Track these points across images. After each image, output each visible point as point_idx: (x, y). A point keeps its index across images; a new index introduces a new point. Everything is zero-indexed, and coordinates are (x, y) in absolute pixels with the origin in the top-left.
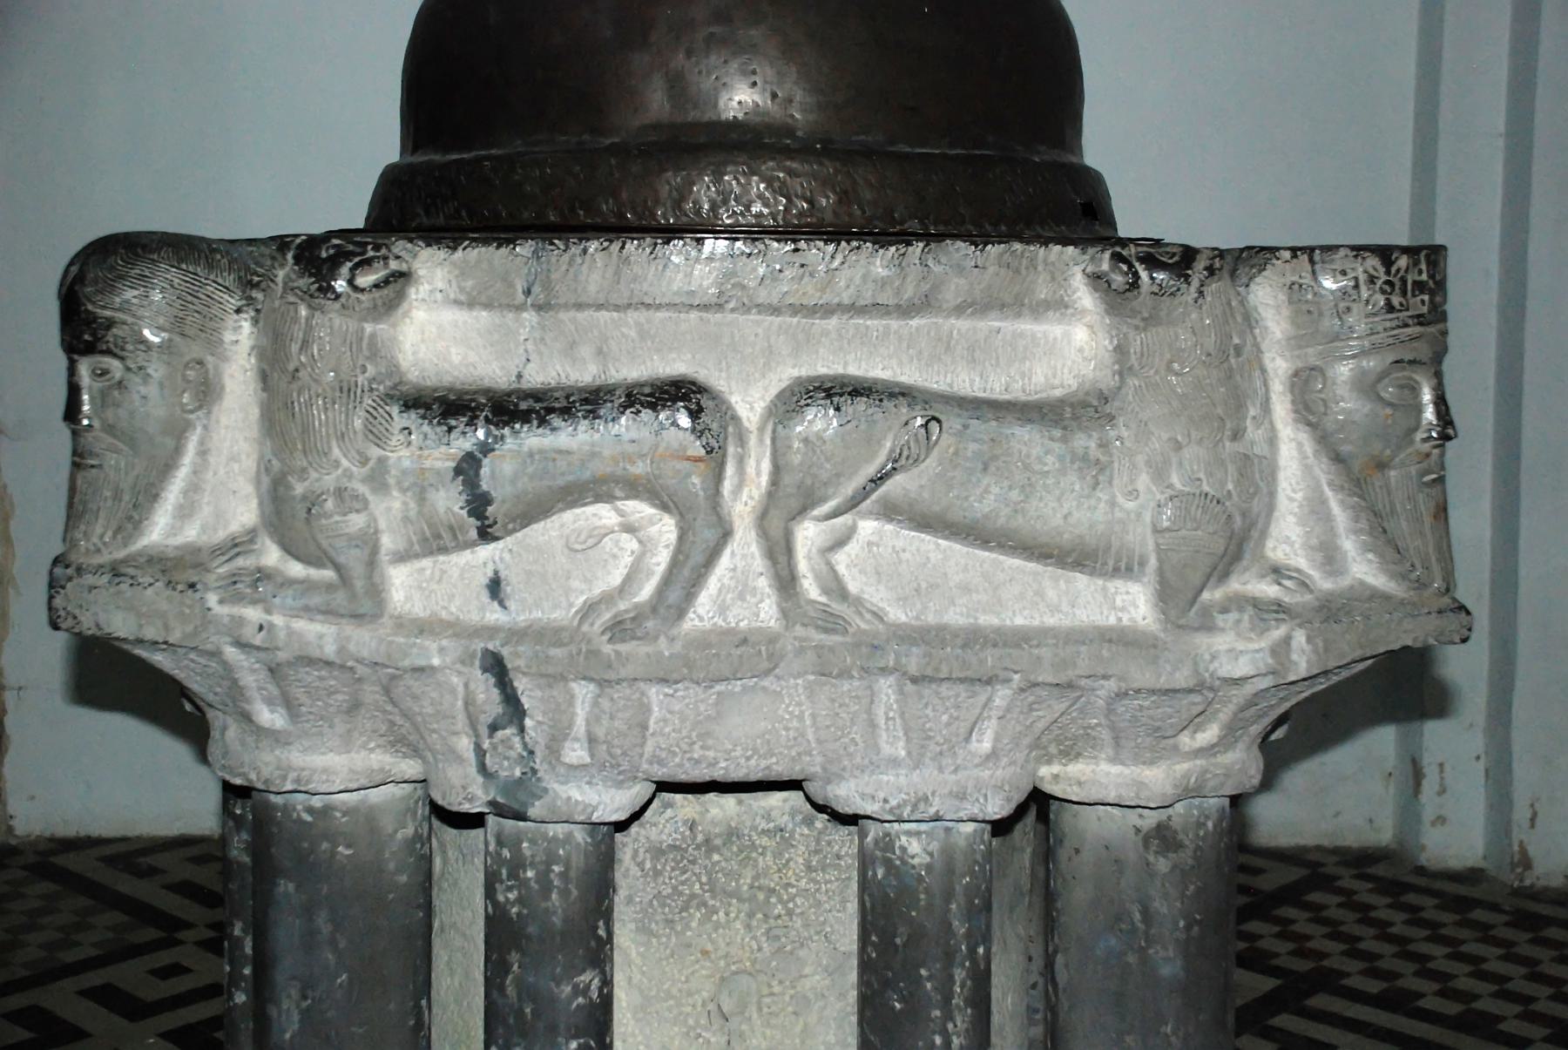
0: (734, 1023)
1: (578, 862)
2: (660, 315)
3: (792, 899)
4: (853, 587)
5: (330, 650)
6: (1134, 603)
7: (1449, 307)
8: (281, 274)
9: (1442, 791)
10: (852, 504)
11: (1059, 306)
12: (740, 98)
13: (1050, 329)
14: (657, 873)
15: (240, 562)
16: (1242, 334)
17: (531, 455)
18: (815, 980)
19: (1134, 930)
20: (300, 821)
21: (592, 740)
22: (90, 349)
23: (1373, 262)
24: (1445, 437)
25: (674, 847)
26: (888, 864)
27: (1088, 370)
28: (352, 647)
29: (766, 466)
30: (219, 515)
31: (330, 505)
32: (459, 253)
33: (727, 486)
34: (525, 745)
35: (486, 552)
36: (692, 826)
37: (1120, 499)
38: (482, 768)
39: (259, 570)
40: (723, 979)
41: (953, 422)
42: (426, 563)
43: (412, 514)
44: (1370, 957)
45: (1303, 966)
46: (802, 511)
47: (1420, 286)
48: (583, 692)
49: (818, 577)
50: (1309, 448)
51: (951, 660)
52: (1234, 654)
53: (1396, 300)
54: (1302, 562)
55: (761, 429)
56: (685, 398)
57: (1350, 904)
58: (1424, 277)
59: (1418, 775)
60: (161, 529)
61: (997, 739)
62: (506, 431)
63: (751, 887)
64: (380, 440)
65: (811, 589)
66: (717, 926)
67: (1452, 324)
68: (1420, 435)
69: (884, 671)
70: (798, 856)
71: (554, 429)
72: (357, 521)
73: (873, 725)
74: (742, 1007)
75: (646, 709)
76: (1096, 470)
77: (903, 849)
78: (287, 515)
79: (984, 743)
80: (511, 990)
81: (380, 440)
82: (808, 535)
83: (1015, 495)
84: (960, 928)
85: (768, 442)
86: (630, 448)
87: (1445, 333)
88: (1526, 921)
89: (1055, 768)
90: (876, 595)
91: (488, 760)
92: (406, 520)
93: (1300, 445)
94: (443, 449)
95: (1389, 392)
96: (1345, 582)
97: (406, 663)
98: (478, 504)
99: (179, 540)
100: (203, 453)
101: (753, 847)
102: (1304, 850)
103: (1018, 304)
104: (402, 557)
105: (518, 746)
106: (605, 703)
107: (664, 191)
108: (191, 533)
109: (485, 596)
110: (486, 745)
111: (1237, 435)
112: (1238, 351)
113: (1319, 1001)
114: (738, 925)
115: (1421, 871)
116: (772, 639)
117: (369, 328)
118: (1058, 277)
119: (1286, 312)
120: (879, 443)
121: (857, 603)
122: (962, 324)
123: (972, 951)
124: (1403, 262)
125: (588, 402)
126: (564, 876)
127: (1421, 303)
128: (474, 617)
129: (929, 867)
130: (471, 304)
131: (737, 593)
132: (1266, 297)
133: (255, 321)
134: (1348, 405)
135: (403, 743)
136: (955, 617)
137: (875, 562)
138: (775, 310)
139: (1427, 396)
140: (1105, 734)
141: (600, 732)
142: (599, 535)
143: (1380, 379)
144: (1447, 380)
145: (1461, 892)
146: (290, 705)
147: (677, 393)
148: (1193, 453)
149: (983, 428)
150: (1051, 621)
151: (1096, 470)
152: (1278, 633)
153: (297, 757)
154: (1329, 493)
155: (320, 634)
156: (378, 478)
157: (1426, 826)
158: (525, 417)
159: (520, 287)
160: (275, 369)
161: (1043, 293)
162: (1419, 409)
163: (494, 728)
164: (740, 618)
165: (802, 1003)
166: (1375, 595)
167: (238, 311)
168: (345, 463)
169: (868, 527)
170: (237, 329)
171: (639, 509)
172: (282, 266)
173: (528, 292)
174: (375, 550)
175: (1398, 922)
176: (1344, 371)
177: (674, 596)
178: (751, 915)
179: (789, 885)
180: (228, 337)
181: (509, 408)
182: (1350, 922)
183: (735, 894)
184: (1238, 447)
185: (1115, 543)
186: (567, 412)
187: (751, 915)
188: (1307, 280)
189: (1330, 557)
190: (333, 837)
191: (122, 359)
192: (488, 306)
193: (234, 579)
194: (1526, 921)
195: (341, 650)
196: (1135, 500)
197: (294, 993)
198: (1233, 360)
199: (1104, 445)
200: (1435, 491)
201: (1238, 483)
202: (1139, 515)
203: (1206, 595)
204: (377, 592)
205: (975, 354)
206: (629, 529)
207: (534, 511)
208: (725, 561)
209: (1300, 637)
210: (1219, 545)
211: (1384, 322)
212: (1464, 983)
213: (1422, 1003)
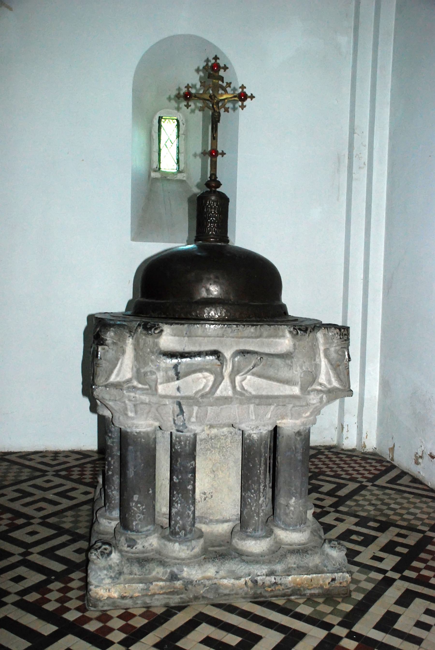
0: (216, 472)
1: (191, 440)
2: (212, 338)
3: (228, 448)
4: (246, 388)
5: (147, 401)
6: (296, 390)
7: (350, 338)
8: (139, 330)
9: (348, 431)
10: (246, 373)
11: (284, 336)
12: (215, 290)
13: (281, 340)
15: (129, 385)
16: (316, 342)
18: (231, 464)
19: (293, 451)
20: (134, 435)
21: (197, 417)
22: (102, 344)
23: (338, 330)
24: (349, 361)
25: (204, 439)
26: (250, 439)
27: (288, 348)
28: (152, 400)
29: (231, 366)
30: (124, 376)
31: (149, 374)
32: (172, 326)
33: (224, 370)
34: (183, 418)
35: (177, 383)
36: (208, 435)
37: (294, 372)
38: (175, 423)
39: (133, 386)
40: (214, 464)
41: (265, 358)
42: (165, 385)
43: (165, 375)
44: (331, 468)
45: (317, 470)
46: (238, 374)
47: (345, 334)
48: (196, 408)
49: (239, 386)
50: (327, 362)
51: (264, 400)
52: (313, 399)
53: (341, 337)
54: (325, 383)
55: (230, 359)
56: (217, 354)
57: (327, 457)
59: (343, 428)
60: (113, 378)
61: (271, 416)
63: (220, 446)
65: (238, 388)
66: (213, 454)
67: (350, 340)
68: (345, 361)
69: (252, 403)
70: (229, 440)
72: (154, 377)
73: (249, 413)
74: (218, 469)
75: (207, 411)
76: (290, 367)
78: (140, 375)
79: (269, 416)
80: (178, 465)
82: (238, 378)
83: (276, 371)
84: (263, 451)
85: (231, 361)
86: (207, 363)
87: (349, 342)
88: (364, 459)
89: (280, 421)
90: (250, 390)
91: (176, 422)
92: (163, 376)
93: (325, 362)
95: (340, 353)
96: (332, 386)
97: (162, 403)
98: (177, 374)
99: (116, 380)
100: (121, 364)
101: (220, 438)
102: (317, 446)
103: (276, 336)
104: (161, 383)
105: (182, 418)
106: (200, 411)
107: (206, 311)
108: (118, 379)
109: (176, 390)
111: (315, 360)
112: (315, 345)
113: (321, 477)
115: (343, 450)
116: (231, 398)
117: (156, 340)
118: (283, 331)
119: (323, 338)
120: (252, 362)
121: (246, 391)
122: (266, 340)
124: (343, 330)
125: (199, 354)
126: (189, 443)
127: (345, 337)
128: (174, 394)
129: (258, 440)
130: (175, 335)
131: (225, 389)
132: (320, 335)
133: (132, 339)
134: (333, 355)
135: (156, 419)
136: (264, 393)
137: (250, 383)
138: (233, 337)
139: (346, 353)
140: (290, 414)
141: (198, 416)
142: (199, 379)
143: (339, 350)
144: (350, 350)
145: (351, 454)
146: (136, 412)
147: (216, 353)
148: (307, 364)
149: (270, 359)
150: (281, 394)
151: (290, 367)
152: (321, 395)
153: (135, 422)
154: (330, 370)
155: (146, 398)
156: (158, 369)
157: (344, 440)
159: (185, 332)
160: (136, 348)
161: (281, 334)
162: (345, 356)
163: (178, 416)
164: (225, 394)
165: (229, 468)
166: (337, 389)
167: (129, 337)
168: (152, 366)
169: (249, 377)
170: (129, 340)
171: (207, 374)
172: (140, 329)
173: (186, 334)
174: (157, 381)
175: (338, 461)
176: (332, 349)
177: (213, 390)
179: (227, 446)
180: (127, 342)
181: (183, 355)
183: (217, 448)
184: (315, 362)
185: (293, 380)
187: (219, 452)
188: (327, 333)
189: (330, 382)
190: (141, 438)
191: (108, 346)
192: (178, 336)
193: (129, 387)
194: (364, 459)
195: (149, 401)
196: (297, 372)
197: (133, 468)
198: (314, 348)
199: (292, 362)
200: (347, 370)
201: (315, 369)
202: (298, 375)
203: (309, 389)
204: (156, 390)
205: (269, 345)
206: (205, 378)
207: (187, 374)
208: (223, 383)
209: (324, 396)
210: (311, 380)
211: (339, 341)
212: (351, 472)
213: (342, 476)
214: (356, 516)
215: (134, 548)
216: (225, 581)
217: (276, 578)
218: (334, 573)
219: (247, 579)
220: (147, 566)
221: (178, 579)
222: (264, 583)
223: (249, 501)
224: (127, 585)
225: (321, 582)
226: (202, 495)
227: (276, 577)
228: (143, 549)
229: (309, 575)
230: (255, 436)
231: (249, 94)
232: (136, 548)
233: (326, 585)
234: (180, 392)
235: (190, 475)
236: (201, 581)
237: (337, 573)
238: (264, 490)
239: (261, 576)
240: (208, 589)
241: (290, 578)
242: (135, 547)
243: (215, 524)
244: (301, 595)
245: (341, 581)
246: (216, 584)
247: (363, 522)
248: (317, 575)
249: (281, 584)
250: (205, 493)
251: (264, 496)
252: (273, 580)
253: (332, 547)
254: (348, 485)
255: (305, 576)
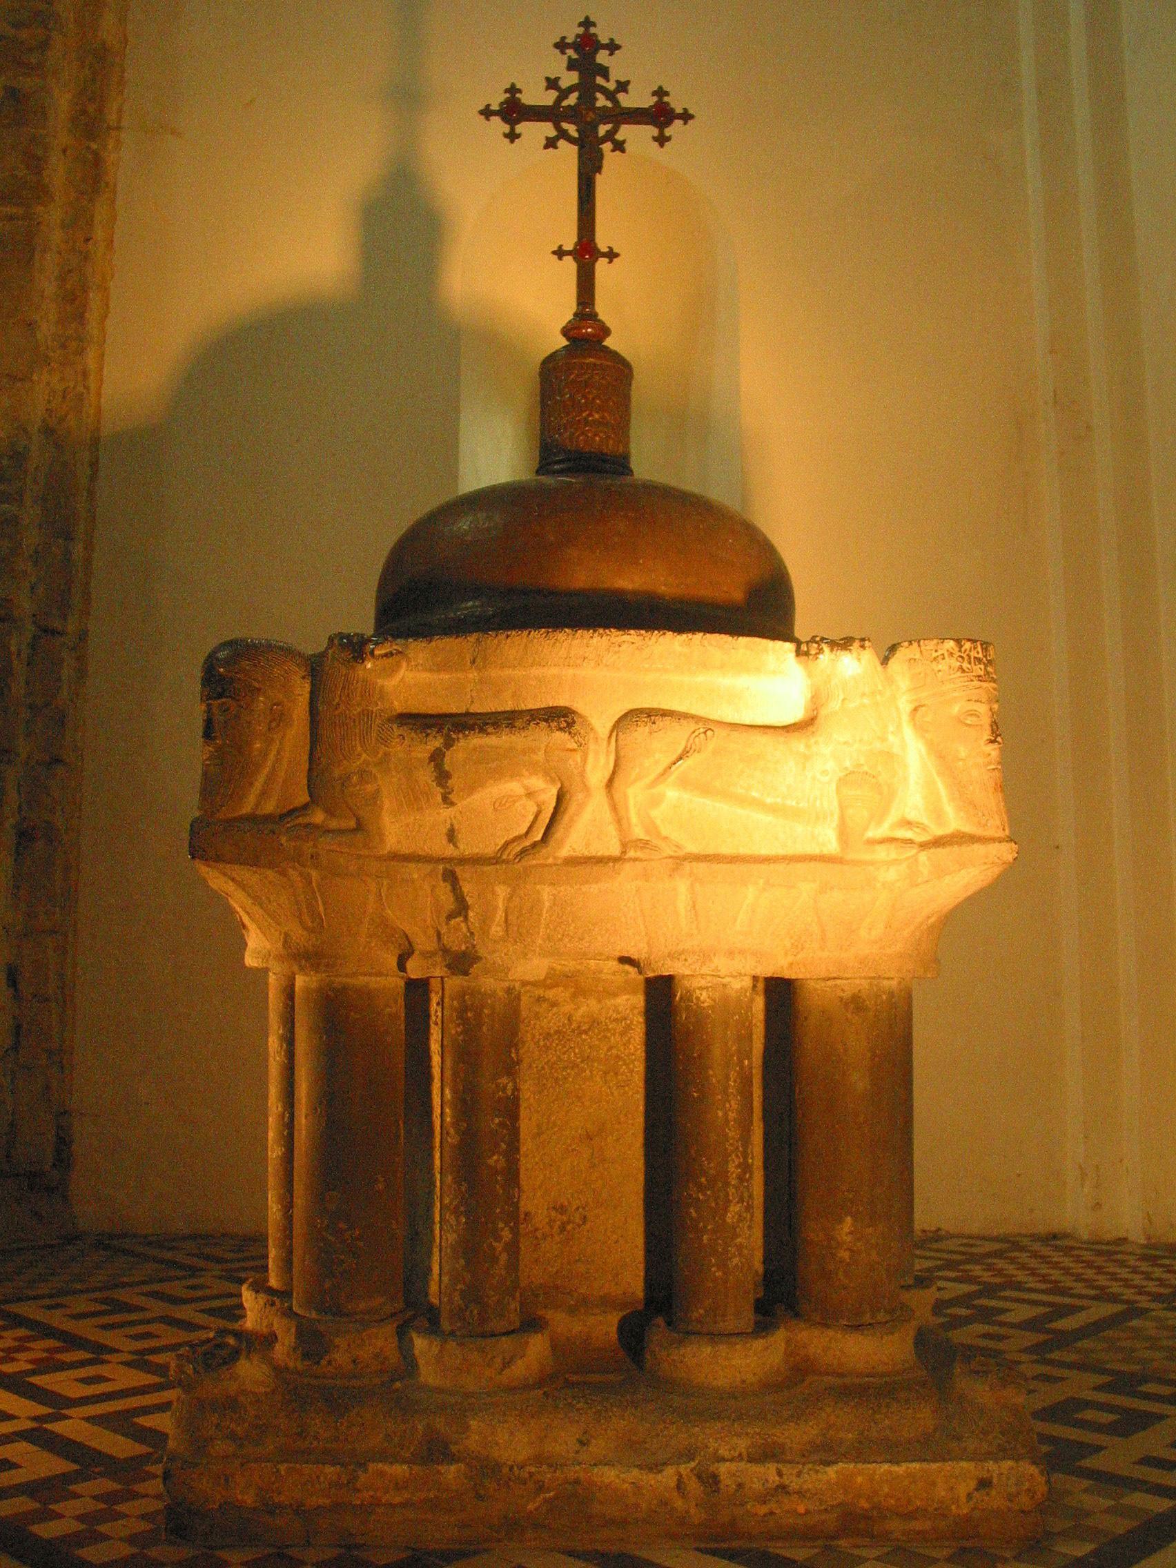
14: (548, 1048)
17: (474, 749)
32: (433, 644)
34: (468, 928)
45: (998, 1280)
53: (966, 665)
54: (925, 821)
57: (1035, 1255)
58: (980, 655)
62: (461, 735)
64: (385, 742)
71: (488, 734)
77: (698, 998)
81: (385, 742)
94: (423, 746)
101: (608, 1030)
105: (465, 930)
110: (444, 930)
114: (598, 1079)
123: (741, 1063)
142: (512, 799)
158: (472, 728)
163: (450, 917)
178: (606, 1073)
182: (1033, 1263)
186: (496, 725)
187: (606, 1073)
189: (938, 815)
214: (1104, 1372)
215: (323, 1362)
216: (610, 1475)
217: (785, 1469)
218: (986, 1460)
219: (684, 1469)
220: (356, 1410)
221: (452, 1458)
222: (740, 1485)
223: (694, 1214)
224: (282, 1468)
225: (942, 1493)
226: (553, 1214)
227: (780, 1466)
228: (352, 1366)
229: (897, 1463)
230: (704, 995)
231: (668, 132)
232: (329, 1362)
233: (956, 1501)
234: (455, 845)
235: (497, 1120)
236: (528, 1469)
237: (996, 1460)
238: (741, 1179)
239: (732, 1460)
240: (556, 1498)
241: (832, 1472)
242: (327, 1358)
243: (596, 1311)
244: (872, 1537)
245: (1013, 1489)
246: (577, 1482)
247: (1124, 1383)
248: (925, 1465)
249: (801, 1493)
250: (562, 1209)
251: (741, 1200)
252: (774, 1479)
253: (977, 1372)
254: (1089, 1308)
255: (886, 1466)
